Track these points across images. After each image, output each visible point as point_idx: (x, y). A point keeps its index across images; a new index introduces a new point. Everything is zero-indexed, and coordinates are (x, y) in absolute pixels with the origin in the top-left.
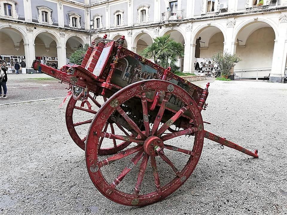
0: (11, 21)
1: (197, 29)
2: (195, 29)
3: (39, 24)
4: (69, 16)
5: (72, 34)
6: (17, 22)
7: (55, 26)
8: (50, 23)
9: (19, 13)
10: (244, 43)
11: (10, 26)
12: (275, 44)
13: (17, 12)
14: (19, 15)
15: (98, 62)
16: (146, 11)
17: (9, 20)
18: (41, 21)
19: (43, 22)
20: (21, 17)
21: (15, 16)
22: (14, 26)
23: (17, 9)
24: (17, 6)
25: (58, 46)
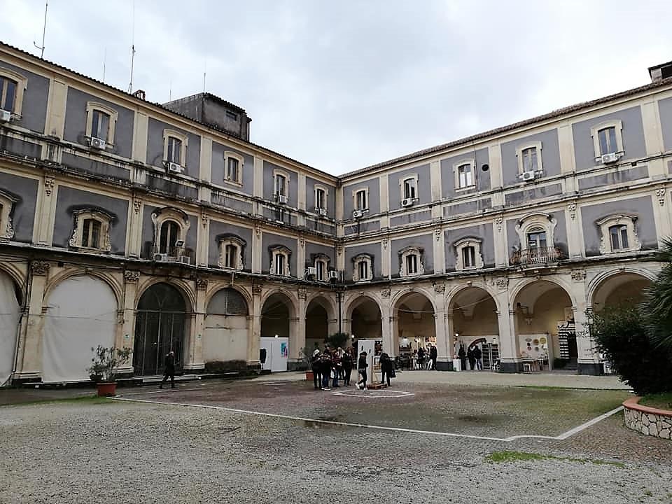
0: (621, 258)
1: (19, 273)
2: (20, 269)
3: (604, 257)
4: (400, 255)
5: (403, 290)
6: (634, 259)
7: (563, 260)
8: (479, 264)
9: (644, 237)
10: (469, 313)
11: (621, 269)
12: (588, 101)
13: (638, 236)
14: (644, 241)
15: (198, 93)
16: (270, 244)
17: (615, 258)
18: (404, 274)
19: (467, 268)
20: (647, 243)
21: (634, 246)
22: (478, 283)
23: (637, 231)
24: (638, 223)
25: (292, 316)
